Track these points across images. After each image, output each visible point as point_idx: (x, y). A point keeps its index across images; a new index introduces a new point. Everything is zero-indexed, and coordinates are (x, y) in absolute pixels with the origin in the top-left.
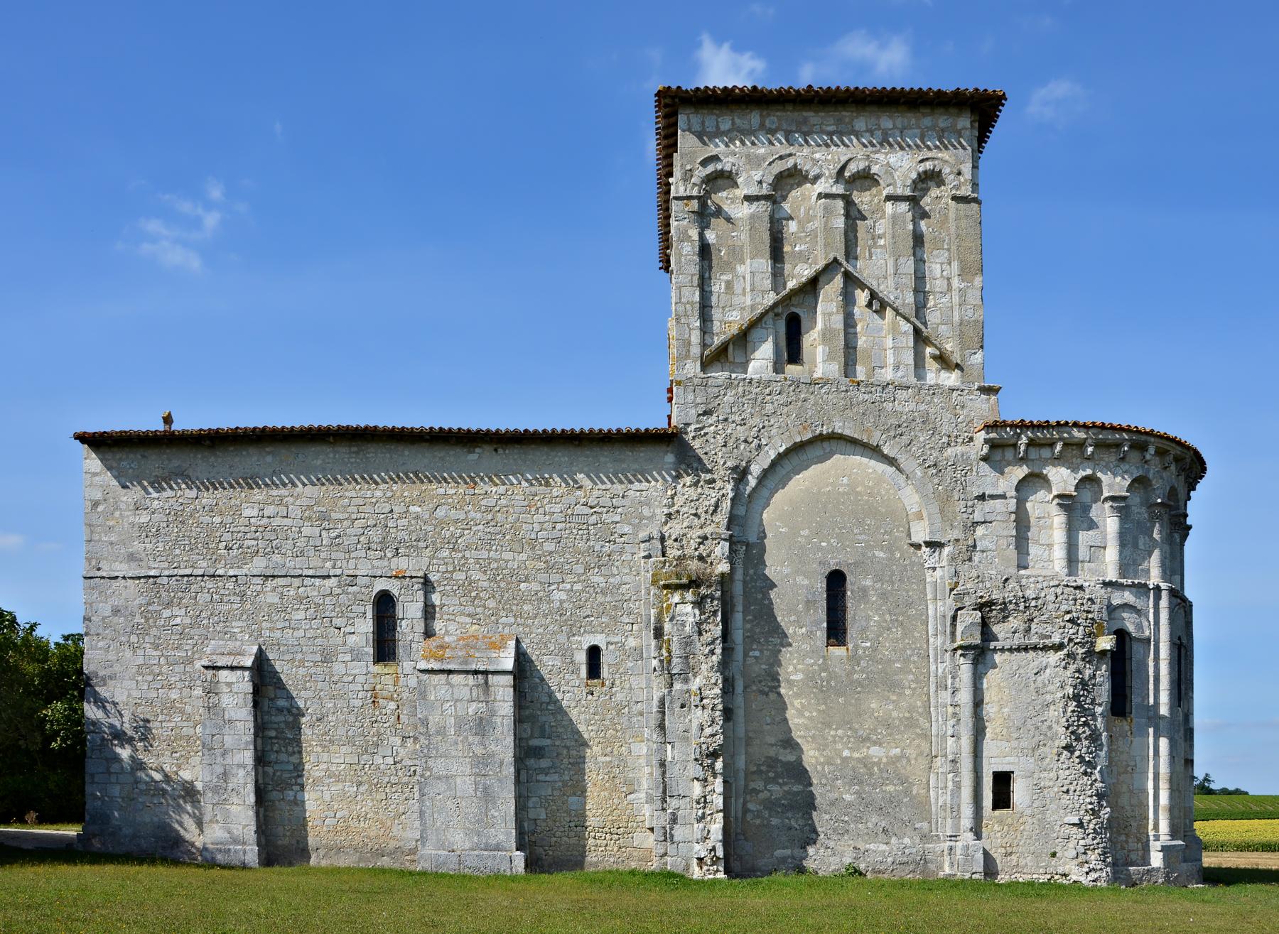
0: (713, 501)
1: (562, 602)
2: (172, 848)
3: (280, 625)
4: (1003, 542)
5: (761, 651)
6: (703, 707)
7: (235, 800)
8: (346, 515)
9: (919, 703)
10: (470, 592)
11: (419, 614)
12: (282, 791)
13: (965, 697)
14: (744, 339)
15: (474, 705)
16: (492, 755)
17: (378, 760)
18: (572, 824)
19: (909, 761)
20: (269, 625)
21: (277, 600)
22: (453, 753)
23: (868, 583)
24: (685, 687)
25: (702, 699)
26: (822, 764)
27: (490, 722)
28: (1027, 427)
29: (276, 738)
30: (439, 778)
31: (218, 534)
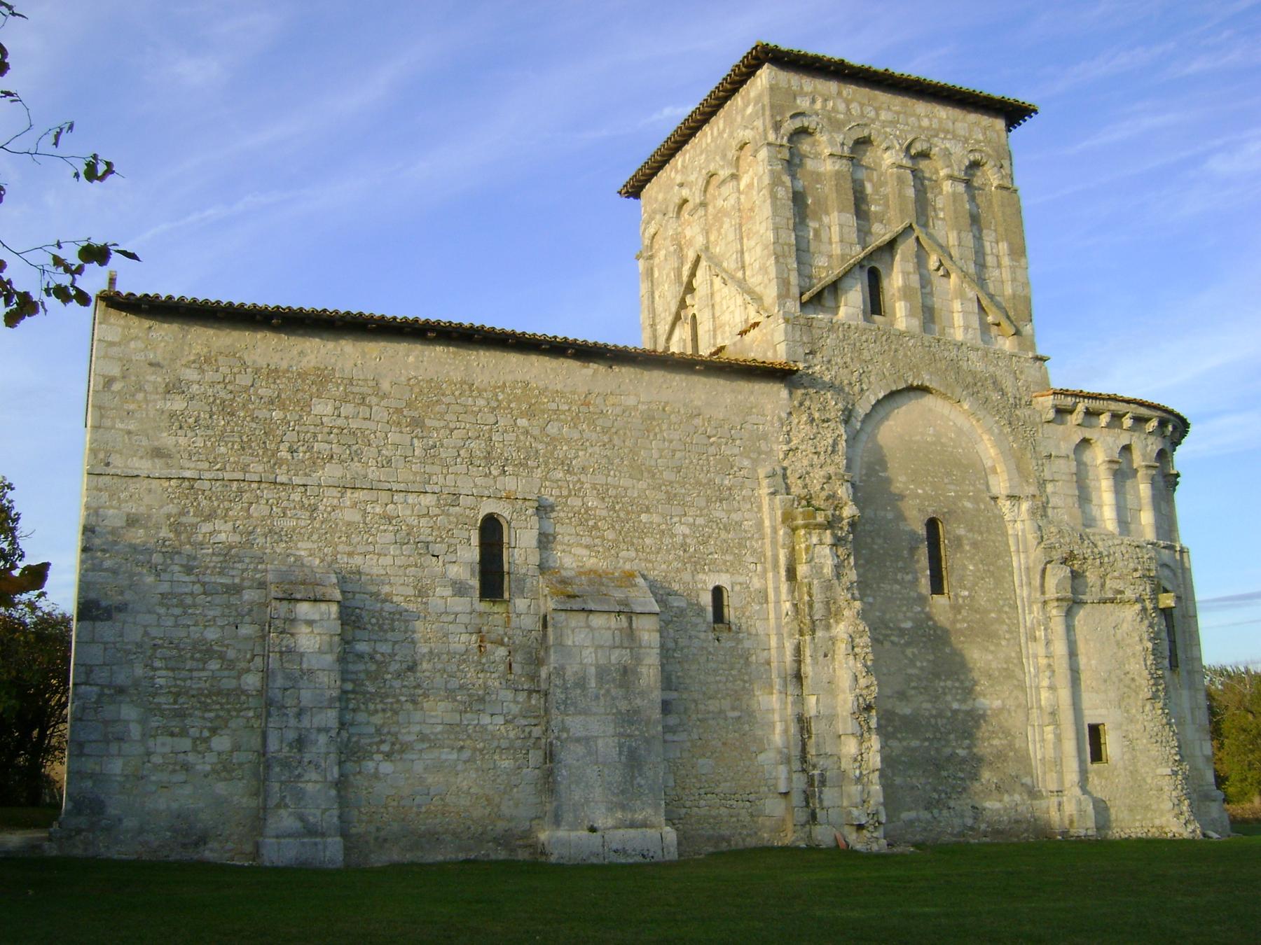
0: (830, 441)
1: (685, 536)
2: (196, 844)
3: (361, 549)
5: (874, 598)
6: (855, 655)
7: (314, 776)
8: (442, 423)
9: (1013, 655)
10: (587, 521)
11: (534, 543)
12: (359, 761)
13: (1060, 648)
14: (835, 287)
15: (617, 652)
16: (637, 711)
17: (486, 720)
18: (702, 791)
19: (1009, 712)
20: (347, 549)
21: (357, 517)
22: (594, 710)
24: (827, 635)
25: (853, 648)
26: (935, 717)
27: (635, 672)
28: (1084, 397)
29: (353, 692)
30: (578, 740)
31: (279, 432)
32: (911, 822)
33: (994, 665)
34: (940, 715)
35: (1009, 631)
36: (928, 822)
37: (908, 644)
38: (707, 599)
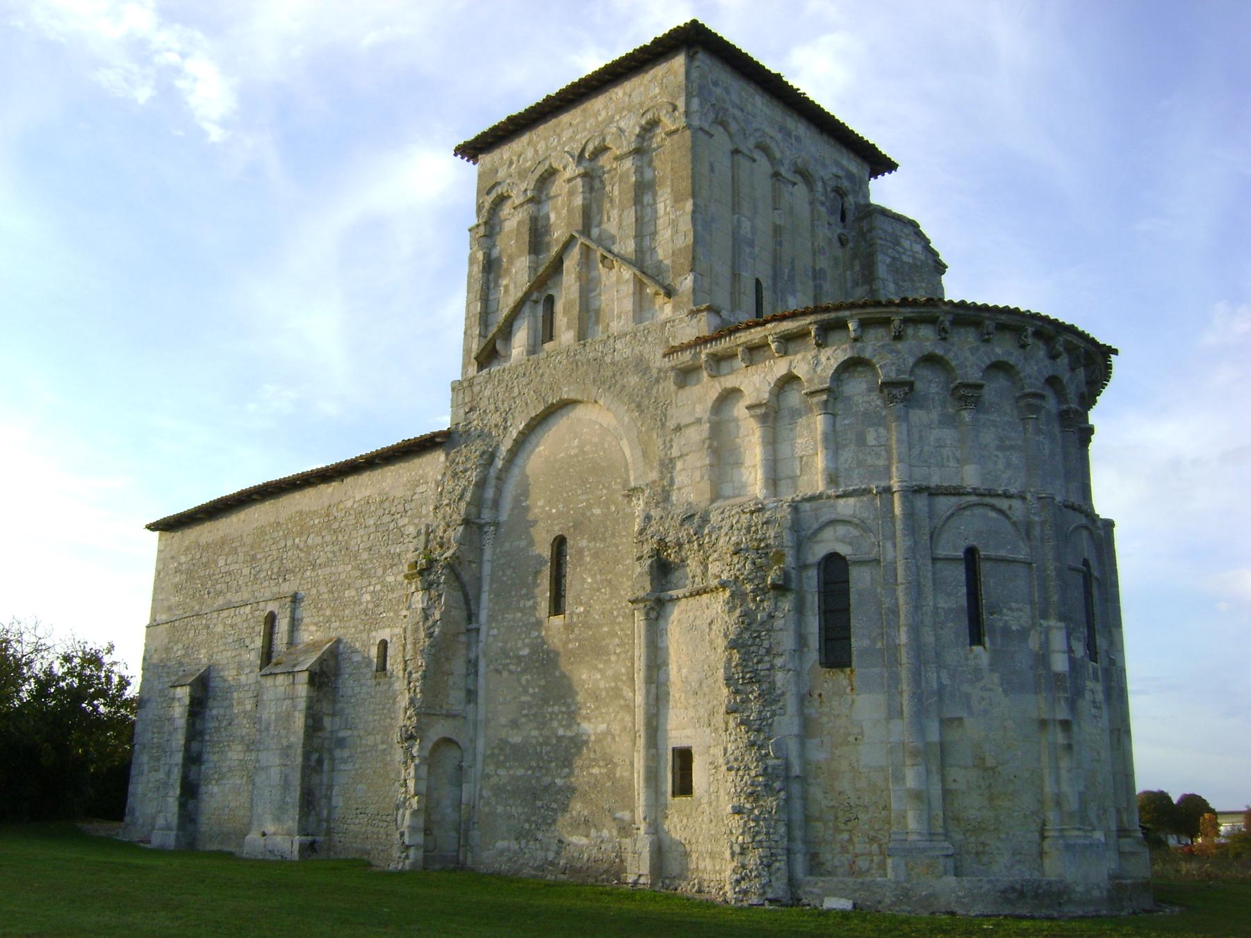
4: (697, 474)
9: (623, 670)
19: (614, 738)
23: (584, 543)
26: (541, 745)
32: (501, 853)
33: (602, 684)
34: (546, 742)
35: (621, 645)
36: (515, 852)
37: (524, 671)
38: (374, 652)
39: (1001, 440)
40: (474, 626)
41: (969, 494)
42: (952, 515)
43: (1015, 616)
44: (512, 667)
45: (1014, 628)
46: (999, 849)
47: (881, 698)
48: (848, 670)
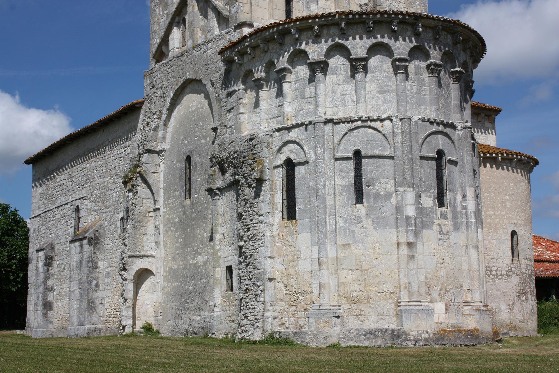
23: (197, 160)
39: (381, 87)
40: (157, 207)
41: (356, 121)
42: (346, 133)
43: (385, 186)
44: (172, 229)
45: (382, 193)
46: (369, 313)
47: (309, 234)
48: (294, 221)
